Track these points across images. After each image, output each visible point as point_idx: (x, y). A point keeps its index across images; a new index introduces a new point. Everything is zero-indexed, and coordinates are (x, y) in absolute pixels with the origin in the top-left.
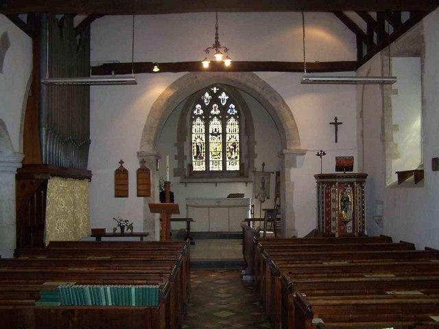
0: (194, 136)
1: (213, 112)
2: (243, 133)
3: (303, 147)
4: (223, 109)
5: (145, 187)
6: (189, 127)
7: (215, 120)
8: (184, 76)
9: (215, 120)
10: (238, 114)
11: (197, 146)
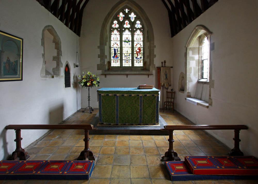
1: (125, 26)
4: (133, 24)
10: (143, 27)
11: (115, 50)
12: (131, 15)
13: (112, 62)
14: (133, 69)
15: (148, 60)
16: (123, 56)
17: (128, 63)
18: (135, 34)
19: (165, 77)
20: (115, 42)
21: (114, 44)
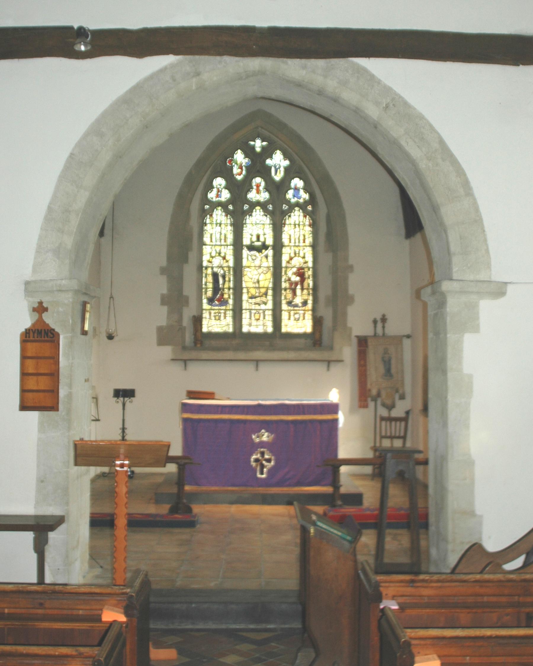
0: (206, 250)
1: (252, 196)
2: (321, 247)
3: (498, 274)
4: (277, 189)
5: (43, 383)
6: (195, 231)
7: (258, 214)
8: (163, 70)
9: (258, 214)
10: (312, 200)
11: (215, 276)
12: (271, 157)
13: (204, 315)
14: (317, 336)
15: (327, 313)
16: (245, 297)
17: (258, 320)
18: (287, 222)
19: (382, 370)
20: (218, 248)
21: (213, 255)
